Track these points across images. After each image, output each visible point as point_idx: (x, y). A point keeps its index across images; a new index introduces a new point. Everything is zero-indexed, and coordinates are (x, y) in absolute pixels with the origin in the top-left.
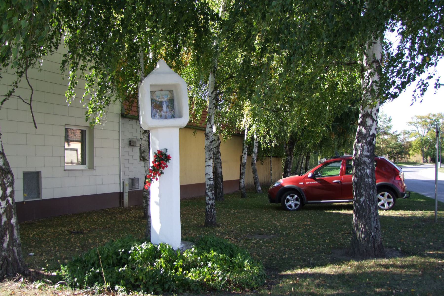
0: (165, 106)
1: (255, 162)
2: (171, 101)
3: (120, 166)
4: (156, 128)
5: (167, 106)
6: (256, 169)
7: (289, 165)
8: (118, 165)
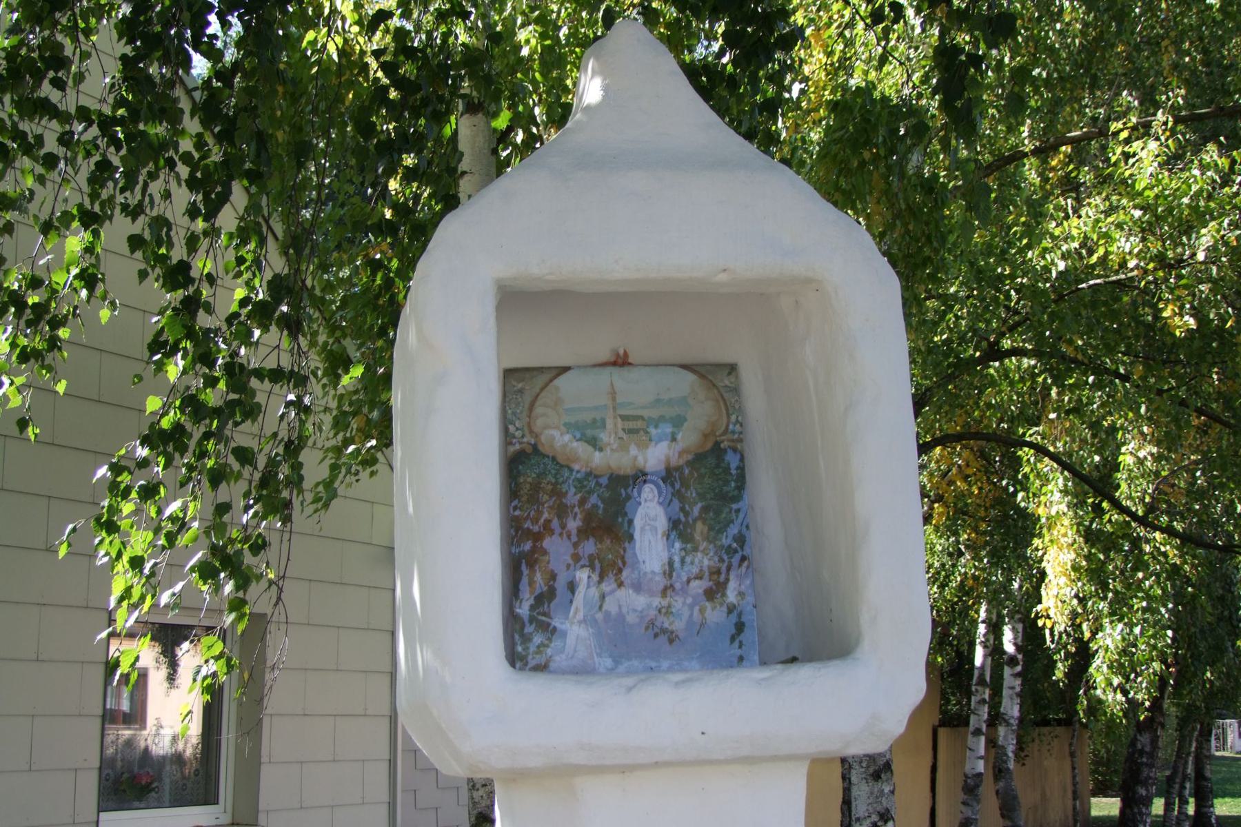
0: (649, 514)
1: (1011, 765)
2: (714, 481)
3: (392, 806)
4: (560, 774)
5: (678, 528)
6: (1015, 798)
7: (1145, 772)
8: (385, 797)
